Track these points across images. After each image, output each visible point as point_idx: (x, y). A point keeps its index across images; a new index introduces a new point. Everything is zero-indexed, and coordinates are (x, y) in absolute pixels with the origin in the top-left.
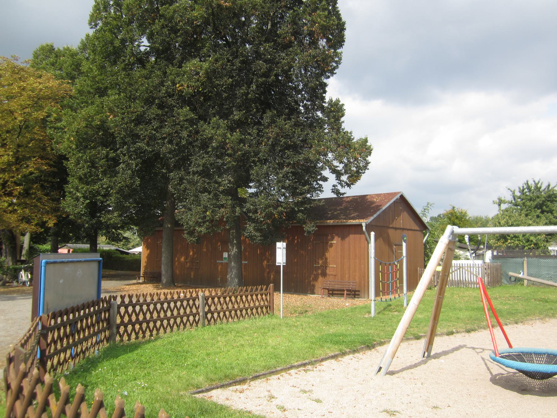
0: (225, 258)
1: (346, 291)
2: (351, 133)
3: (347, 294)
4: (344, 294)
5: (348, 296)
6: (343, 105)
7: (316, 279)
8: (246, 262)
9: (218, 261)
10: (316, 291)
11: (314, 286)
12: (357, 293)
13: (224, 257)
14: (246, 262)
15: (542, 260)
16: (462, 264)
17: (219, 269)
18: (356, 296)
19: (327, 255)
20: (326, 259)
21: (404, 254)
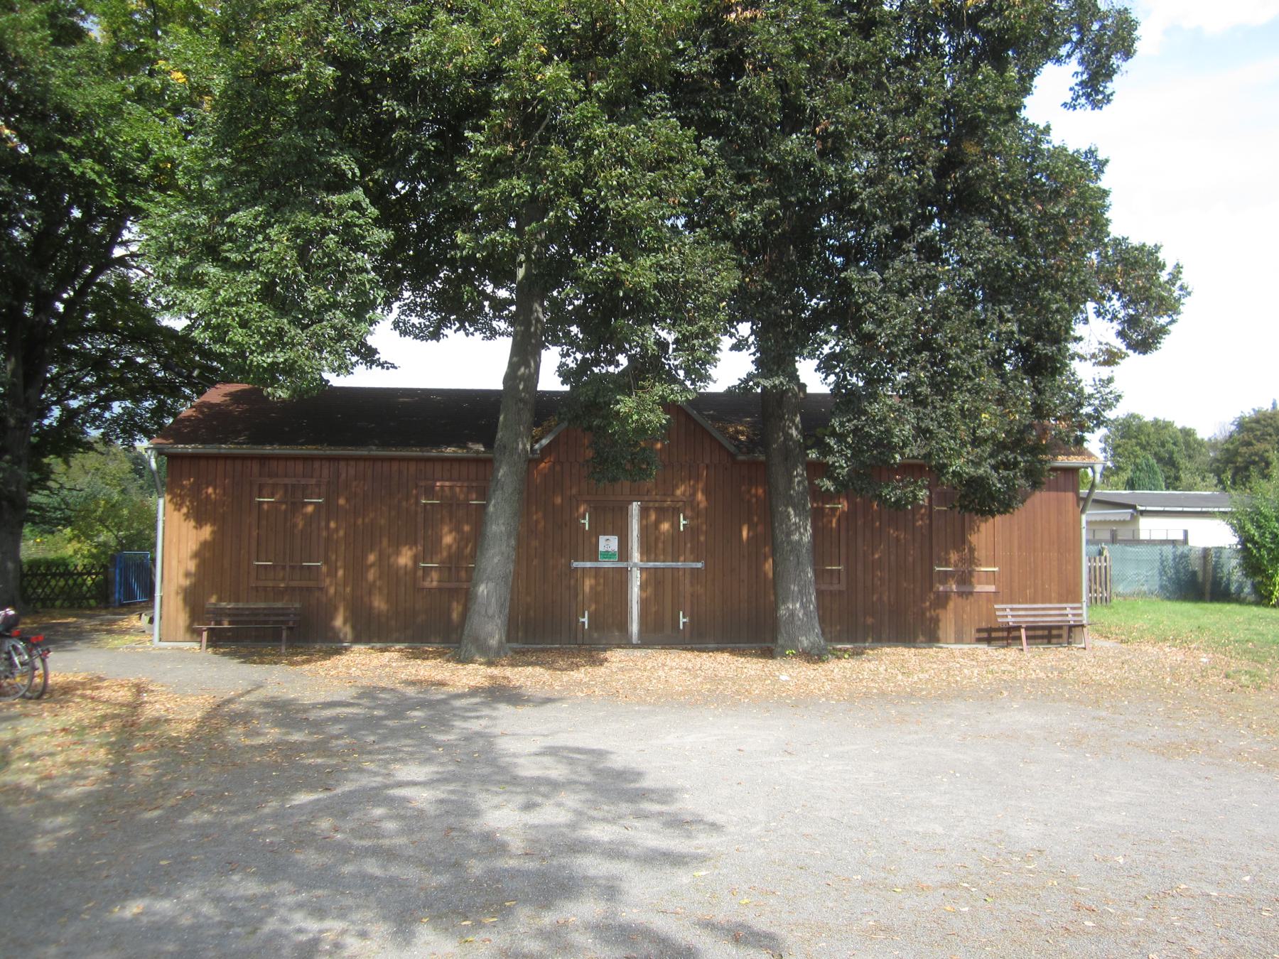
0: (607, 554)
1: (1023, 631)
2: (1156, 349)
3: (1027, 638)
4: (1019, 638)
5: (1032, 641)
6: (1254, 410)
7: (942, 601)
8: (699, 565)
9: (575, 564)
10: (941, 634)
11: (936, 621)
12: (1054, 632)
13: (601, 548)
14: (699, 565)
15: (1129, 549)
16: (979, 630)
17: (587, 589)
18: (1054, 641)
19: (973, 539)
20: (972, 550)
21: (1084, 531)
